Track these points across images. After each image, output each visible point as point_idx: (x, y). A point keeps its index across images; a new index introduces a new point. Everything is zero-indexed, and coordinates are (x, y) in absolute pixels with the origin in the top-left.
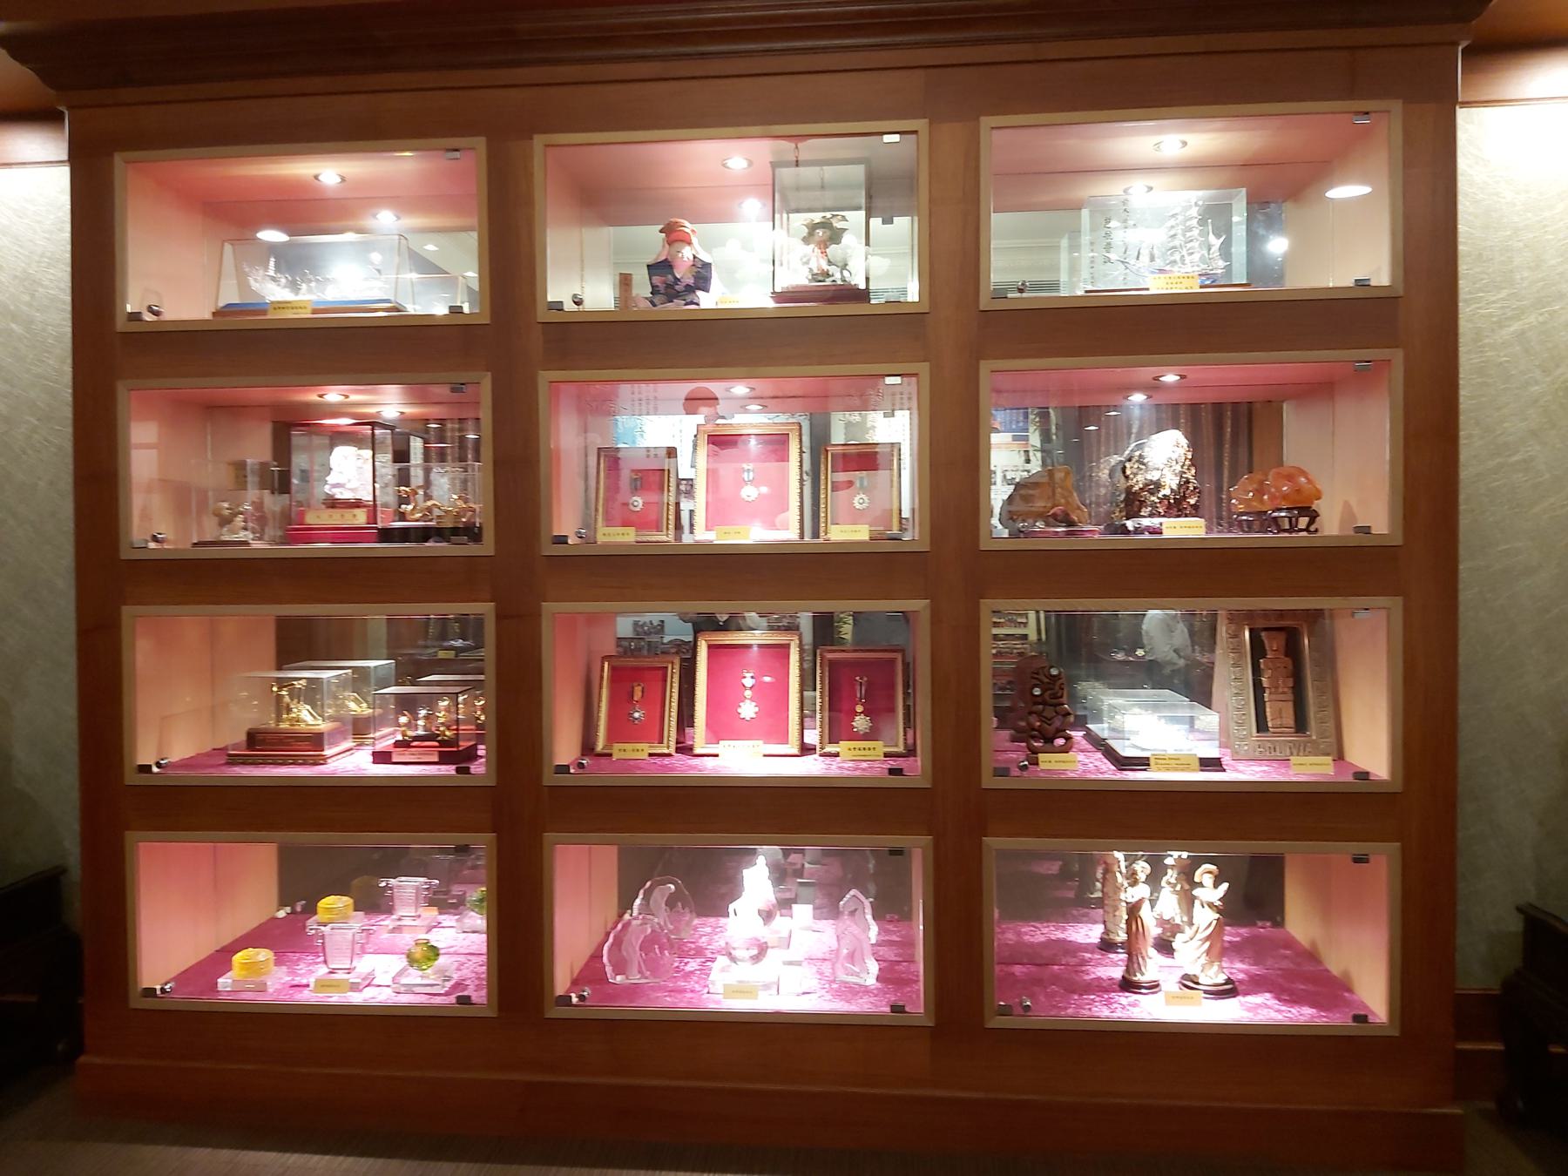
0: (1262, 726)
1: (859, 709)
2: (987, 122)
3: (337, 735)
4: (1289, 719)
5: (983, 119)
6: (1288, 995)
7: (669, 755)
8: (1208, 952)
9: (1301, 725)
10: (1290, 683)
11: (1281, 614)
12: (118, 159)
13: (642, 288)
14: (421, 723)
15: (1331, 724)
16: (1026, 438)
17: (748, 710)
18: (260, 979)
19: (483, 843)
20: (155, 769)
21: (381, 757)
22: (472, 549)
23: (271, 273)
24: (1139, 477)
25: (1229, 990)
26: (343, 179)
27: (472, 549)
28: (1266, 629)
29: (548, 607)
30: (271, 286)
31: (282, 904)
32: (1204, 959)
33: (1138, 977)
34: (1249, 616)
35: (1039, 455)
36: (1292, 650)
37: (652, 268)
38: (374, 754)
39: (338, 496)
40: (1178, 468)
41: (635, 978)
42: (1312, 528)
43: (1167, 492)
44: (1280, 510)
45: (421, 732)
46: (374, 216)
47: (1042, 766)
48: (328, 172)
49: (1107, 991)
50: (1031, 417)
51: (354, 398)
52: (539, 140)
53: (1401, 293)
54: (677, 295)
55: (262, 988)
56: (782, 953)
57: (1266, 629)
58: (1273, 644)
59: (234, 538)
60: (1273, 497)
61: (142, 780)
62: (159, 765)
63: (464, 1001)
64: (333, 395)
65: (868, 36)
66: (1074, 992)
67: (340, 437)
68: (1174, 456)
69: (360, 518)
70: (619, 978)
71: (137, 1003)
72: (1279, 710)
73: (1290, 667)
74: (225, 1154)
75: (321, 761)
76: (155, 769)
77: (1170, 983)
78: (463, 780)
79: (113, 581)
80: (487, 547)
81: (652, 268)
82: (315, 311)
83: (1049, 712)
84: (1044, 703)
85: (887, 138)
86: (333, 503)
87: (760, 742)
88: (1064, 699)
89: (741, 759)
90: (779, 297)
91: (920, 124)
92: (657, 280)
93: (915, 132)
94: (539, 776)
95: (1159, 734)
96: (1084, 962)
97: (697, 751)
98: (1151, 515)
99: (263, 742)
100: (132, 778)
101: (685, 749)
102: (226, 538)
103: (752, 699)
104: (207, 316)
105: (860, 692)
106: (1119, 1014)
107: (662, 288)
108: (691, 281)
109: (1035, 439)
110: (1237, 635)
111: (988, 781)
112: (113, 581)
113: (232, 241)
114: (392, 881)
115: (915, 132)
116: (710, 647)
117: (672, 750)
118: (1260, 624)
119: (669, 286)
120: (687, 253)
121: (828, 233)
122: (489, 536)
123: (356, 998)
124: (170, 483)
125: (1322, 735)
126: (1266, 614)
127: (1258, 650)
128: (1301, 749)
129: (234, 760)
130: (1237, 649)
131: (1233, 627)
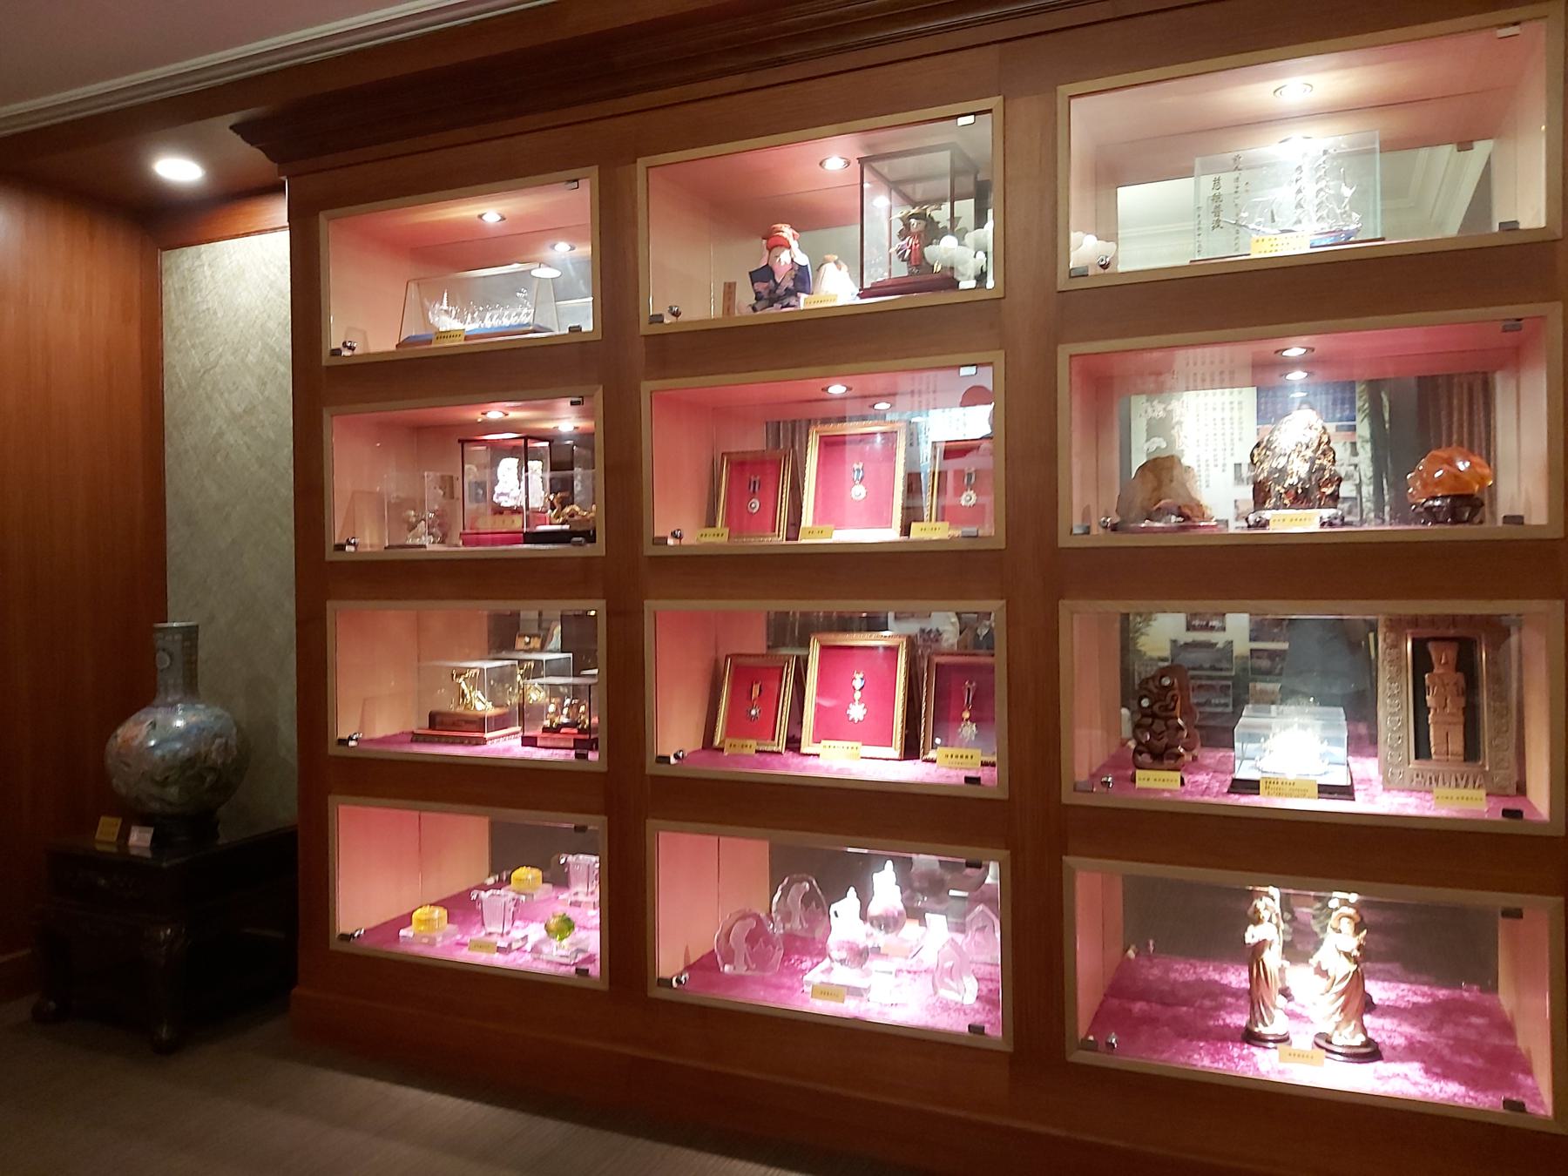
0: (1422, 751)
1: (966, 715)
2: (1064, 90)
3: (500, 722)
4: (1457, 745)
5: (1061, 88)
6: (1439, 1066)
7: (779, 753)
8: (1343, 1008)
9: (1471, 752)
10: (1462, 702)
11: (1453, 620)
12: (322, 216)
13: (745, 296)
14: (565, 711)
15: (1511, 754)
16: (1354, 429)
17: (857, 712)
18: (431, 934)
19: (597, 824)
20: (673, 761)
21: (528, 741)
22: (589, 550)
23: (445, 307)
24: (1266, 466)
25: (1370, 1053)
26: (503, 219)
27: (589, 550)
28: (1435, 639)
29: (650, 605)
30: (445, 318)
31: (492, 872)
32: (1338, 1017)
33: (1260, 1029)
34: (1415, 622)
35: (1368, 447)
36: (1466, 665)
37: (755, 276)
38: (523, 738)
39: (504, 504)
40: (1309, 453)
41: (742, 970)
42: (1477, 519)
43: (1295, 480)
44: (1435, 498)
45: (564, 720)
46: (553, 247)
47: (1139, 783)
48: (489, 212)
49: (1224, 1039)
50: (1359, 404)
51: (513, 415)
52: (642, 163)
53: (1559, 235)
54: (779, 299)
55: (432, 943)
56: (904, 963)
57: (1435, 639)
58: (1443, 658)
59: (418, 542)
60: (1425, 485)
61: (661, 770)
62: (676, 756)
63: (582, 973)
64: (494, 414)
65: (946, 17)
66: (1185, 1036)
67: (500, 451)
68: (1305, 441)
69: (518, 523)
70: (727, 968)
71: (335, 945)
72: (1446, 735)
73: (1462, 683)
74: (381, 1086)
75: (483, 741)
76: (673, 761)
77: (1302, 1040)
78: (581, 766)
79: (327, 581)
80: (598, 549)
81: (755, 276)
82: (466, 338)
83: (1159, 726)
84: (1154, 716)
85: (962, 121)
86: (499, 510)
87: (858, 744)
88: (1178, 712)
89: (851, 757)
90: (864, 293)
91: (995, 102)
92: (760, 286)
93: (990, 111)
94: (643, 766)
95: (1294, 755)
96: (1223, 1006)
97: (804, 750)
98: (1276, 507)
99: (442, 723)
100: (652, 768)
101: (794, 744)
102: (410, 542)
103: (860, 701)
104: (393, 348)
105: (967, 698)
106: (1220, 1067)
107: (765, 294)
108: (791, 285)
109: (1364, 428)
110: (1395, 645)
111: (1068, 797)
112: (327, 581)
113: (419, 282)
114: (571, 858)
115: (990, 111)
116: (824, 648)
117: (782, 747)
118: (1425, 633)
119: (772, 292)
120: (785, 257)
121: (923, 223)
122: (601, 537)
123: (499, 960)
124: (376, 500)
125: (1496, 765)
126: (1433, 620)
127: (1422, 663)
128: (1463, 781)
129: (417, 738)
130: (1396, 661)
131: (1393, 636)
